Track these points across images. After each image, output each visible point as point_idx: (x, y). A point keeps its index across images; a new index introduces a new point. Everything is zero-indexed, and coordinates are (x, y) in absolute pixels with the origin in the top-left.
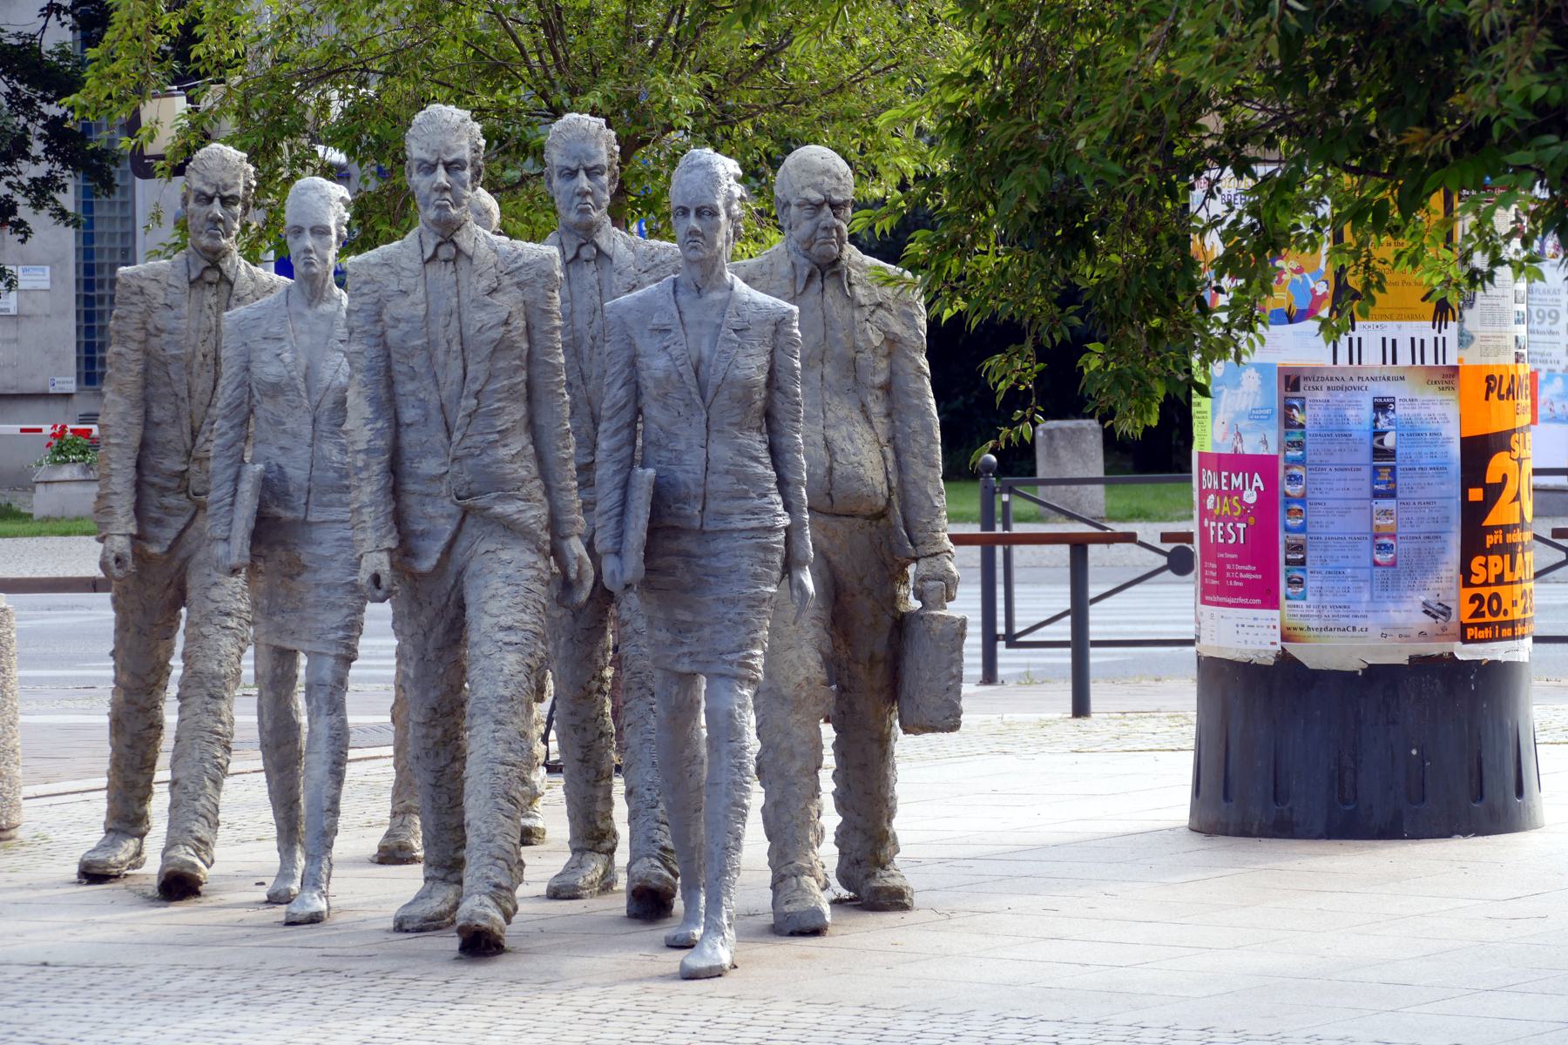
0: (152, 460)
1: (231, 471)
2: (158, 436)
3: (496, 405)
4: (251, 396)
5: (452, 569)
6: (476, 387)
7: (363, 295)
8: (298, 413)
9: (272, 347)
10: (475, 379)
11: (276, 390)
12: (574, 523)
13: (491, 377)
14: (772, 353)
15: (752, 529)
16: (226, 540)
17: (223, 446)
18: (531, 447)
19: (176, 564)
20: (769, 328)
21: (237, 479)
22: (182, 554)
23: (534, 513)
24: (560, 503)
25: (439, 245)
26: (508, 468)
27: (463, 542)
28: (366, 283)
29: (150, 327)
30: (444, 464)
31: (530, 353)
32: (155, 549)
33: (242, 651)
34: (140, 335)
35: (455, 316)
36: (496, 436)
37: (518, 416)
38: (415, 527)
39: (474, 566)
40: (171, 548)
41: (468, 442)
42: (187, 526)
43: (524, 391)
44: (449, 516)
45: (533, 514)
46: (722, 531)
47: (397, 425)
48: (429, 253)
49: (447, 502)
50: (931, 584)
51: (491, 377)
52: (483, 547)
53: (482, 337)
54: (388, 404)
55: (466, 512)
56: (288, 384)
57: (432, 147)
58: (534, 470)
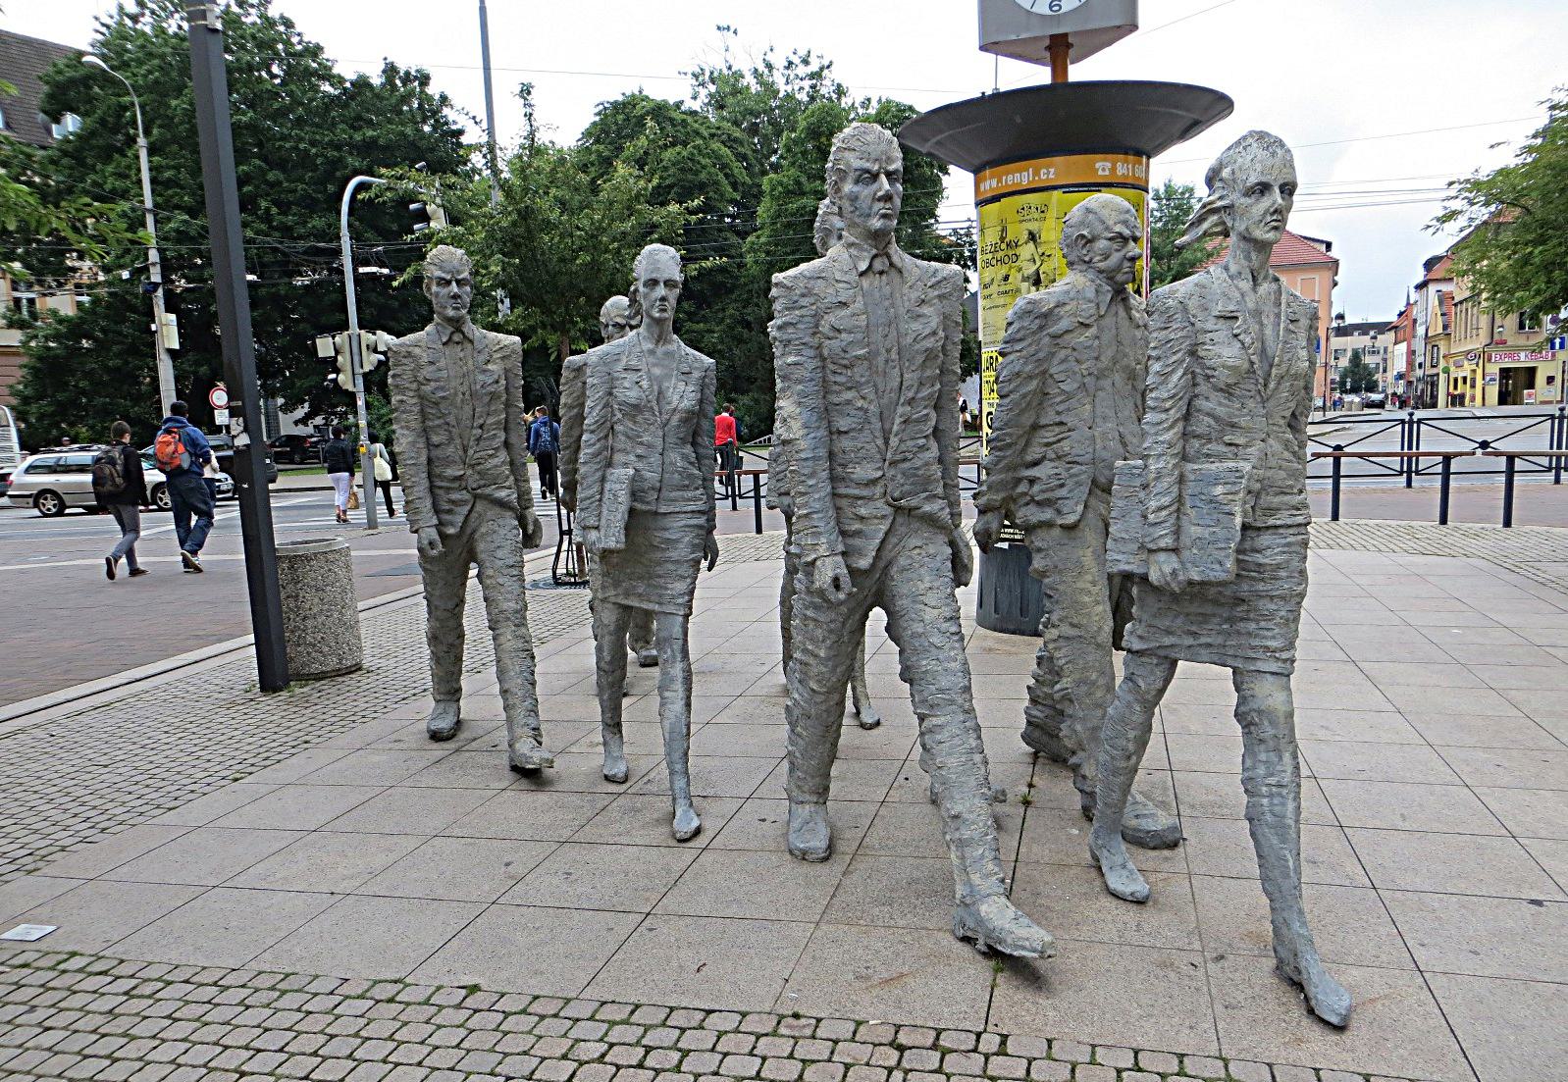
1: (599, 474)
5: (469, 531)
9: (633, 376)
10: (909, 388)
11: (636, 409)
16: (597, 528)
22: (469, 531)
25: (875, 257)
28: (803, 295)
29: (421, 379)
32: (451, 531)
34: (414, 386)
41: (903, 447)
42: (470, 511)
44: (884, 517)
46: (1268, 528)
49: (880, 503)
52: (914, 542)
53: (917, 347)
57: (873, 156)
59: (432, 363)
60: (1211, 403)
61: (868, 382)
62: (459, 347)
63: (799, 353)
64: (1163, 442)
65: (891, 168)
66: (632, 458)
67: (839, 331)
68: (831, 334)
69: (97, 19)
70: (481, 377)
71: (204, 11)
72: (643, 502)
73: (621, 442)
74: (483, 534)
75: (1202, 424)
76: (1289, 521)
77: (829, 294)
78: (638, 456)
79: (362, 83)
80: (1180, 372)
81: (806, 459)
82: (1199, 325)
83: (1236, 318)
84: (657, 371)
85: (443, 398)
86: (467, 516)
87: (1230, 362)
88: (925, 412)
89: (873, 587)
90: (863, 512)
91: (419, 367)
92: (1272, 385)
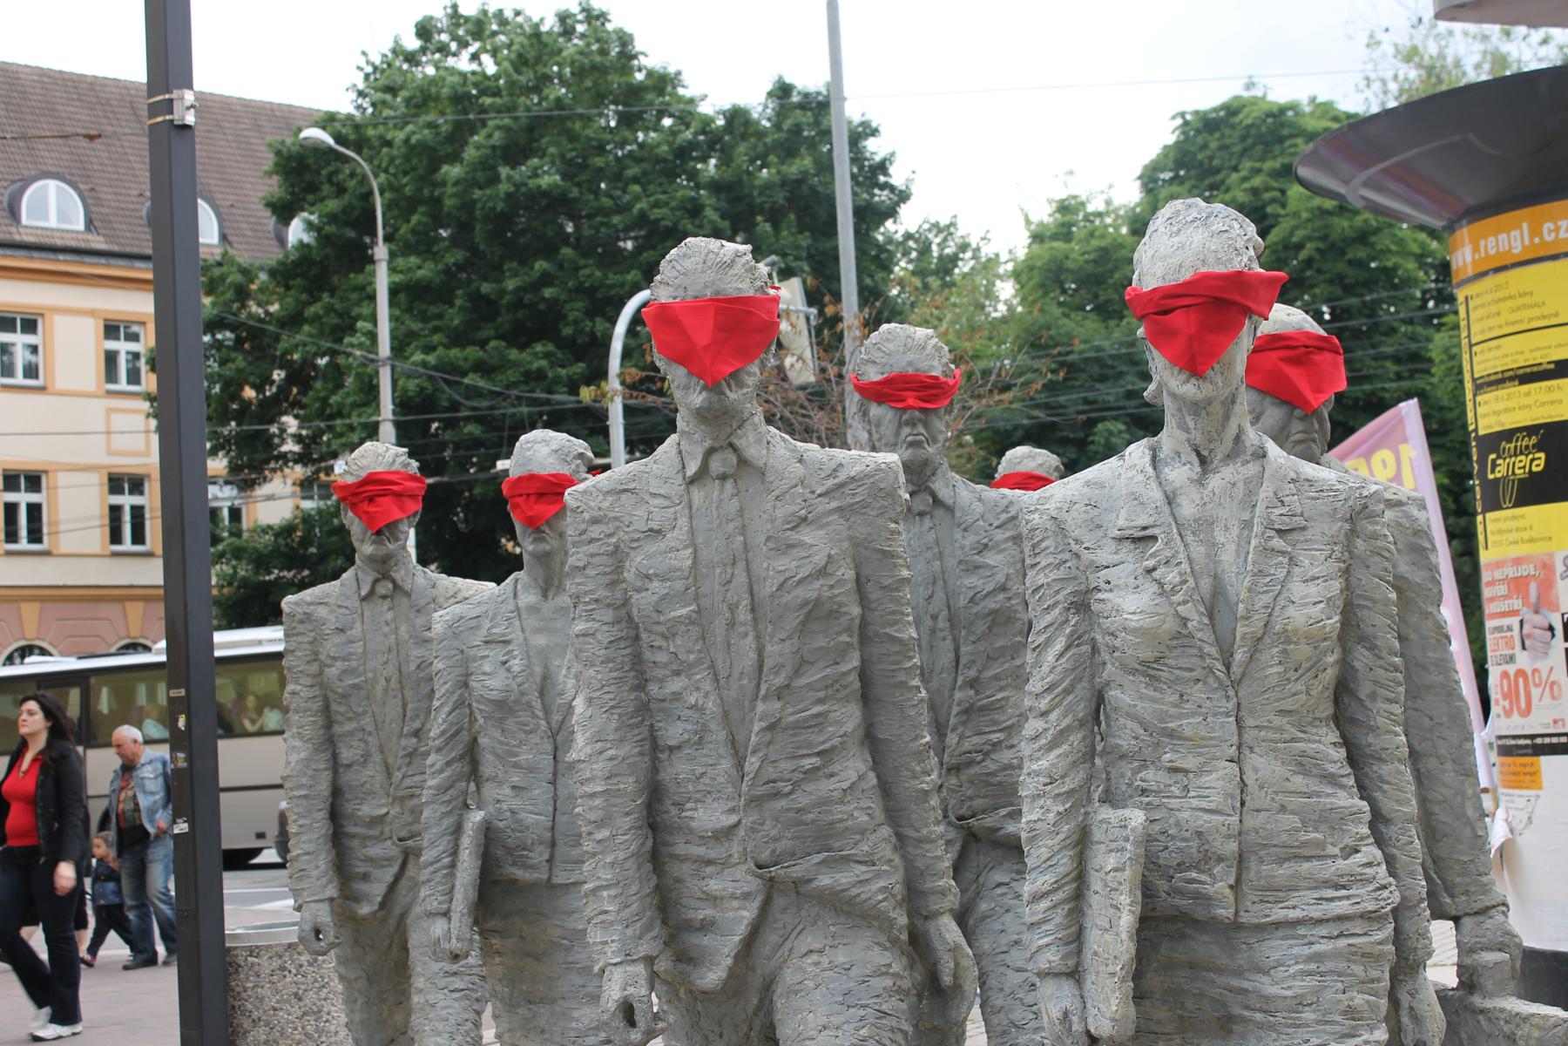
0: (349, 807)
1: (448, 822)
2: (347, 778)
3: (999, 696)
4: (473, 720)
6: (779, 680)
7: (592, 541)
8: (534, 739)
9: (497, 653)
11: (504, 707)
12: (943, 893)
13: (802, 664)
14: (1346, 572)
15: (1341, 918)
17: (437, 788)
18: (872, 775)
19: (393, 922)
20: (1339, 527)
21: (457, 830)
22: (397, 911)
23: (882, 884)
24: (920, 864)
26: (838, 812)
27: (771, 937)
28: (595, 521)
30: (733, 810)
31: (864, 624)
33: (479, 1013)
34: (314, 667)
35: (741, 565)
36: (815, 761)
37: (849, 727)
38: (691, 915)
39: (789, 977)
40: (382, 905)
42: (398, 878)
43: (857, 685)
44: (746, 896)
45: (878, 884)
46: (1278, 925)
47: (655, 749)
48: (692, 469)
49: (740, 872)
50: (1489, 957)
51: (802, 664)
54: (642, 712)
55: (772, 887)
56: (516, 702)
58: (880, 816)
59: (341, 630)
60: (1125, 695)
61: (699, 662)
63: (590, 618)
64: (1038, 774)
66: (508, 791)
67: (648, 577)
68: (639, 584)
69: (364, 53)
71: (171, 101)
72: (526, 867)
75: (1125, 735)
76: (1316, 912)
77: (639, 517)
78: (513, 788)
79: (737, 117)
80: (1059, 645)
81: (593, 795)
82: (1085, 555)
83: (1154, 538)
84: (540, 640)
85: (354, 686)
87: (1135, 621)
90: (714, 886)
92: (1239, 656)
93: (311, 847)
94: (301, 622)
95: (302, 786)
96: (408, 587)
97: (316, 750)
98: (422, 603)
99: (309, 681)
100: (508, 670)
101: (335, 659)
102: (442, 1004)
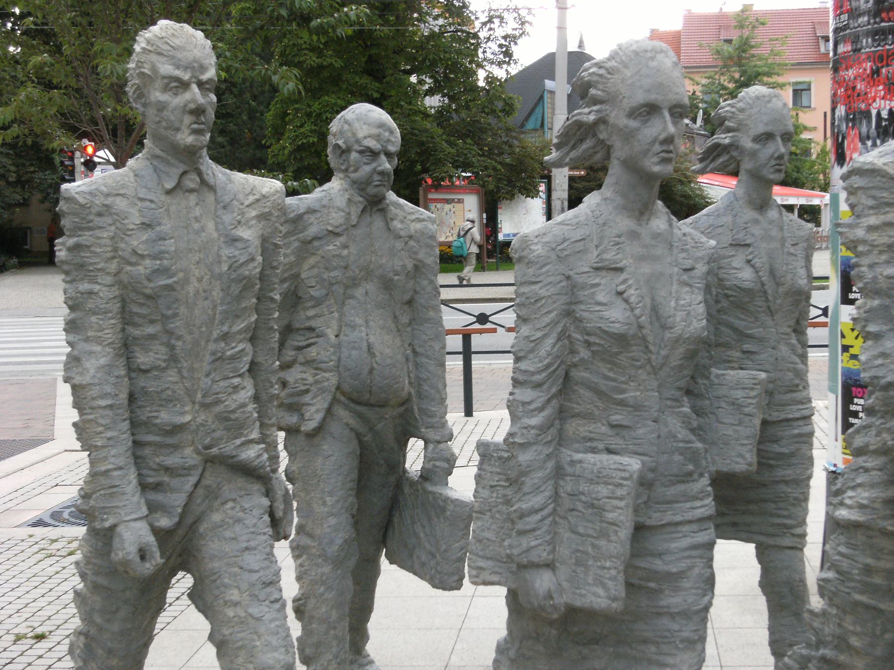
22: (189, 520)
25: (184, 173)
34: (113, 266)
42: (196, 486)
59: (147, 226)
62: (193, 198)
65: (205, 77)
70: (226, 252)
73: (584, 399)
74: (216, 526)
86: (191, 496)
88: (241, 347)
89: (180, 547)
91: (125, 232)
93: (121, 461)
94: (100, 215)
95: (104, 396)
96: (211, 181)
97: (117, 355)
98: (227, 199)
99: (109, 280)
100: (626, 301)
101: (142, 257)
102: (268, 617)
